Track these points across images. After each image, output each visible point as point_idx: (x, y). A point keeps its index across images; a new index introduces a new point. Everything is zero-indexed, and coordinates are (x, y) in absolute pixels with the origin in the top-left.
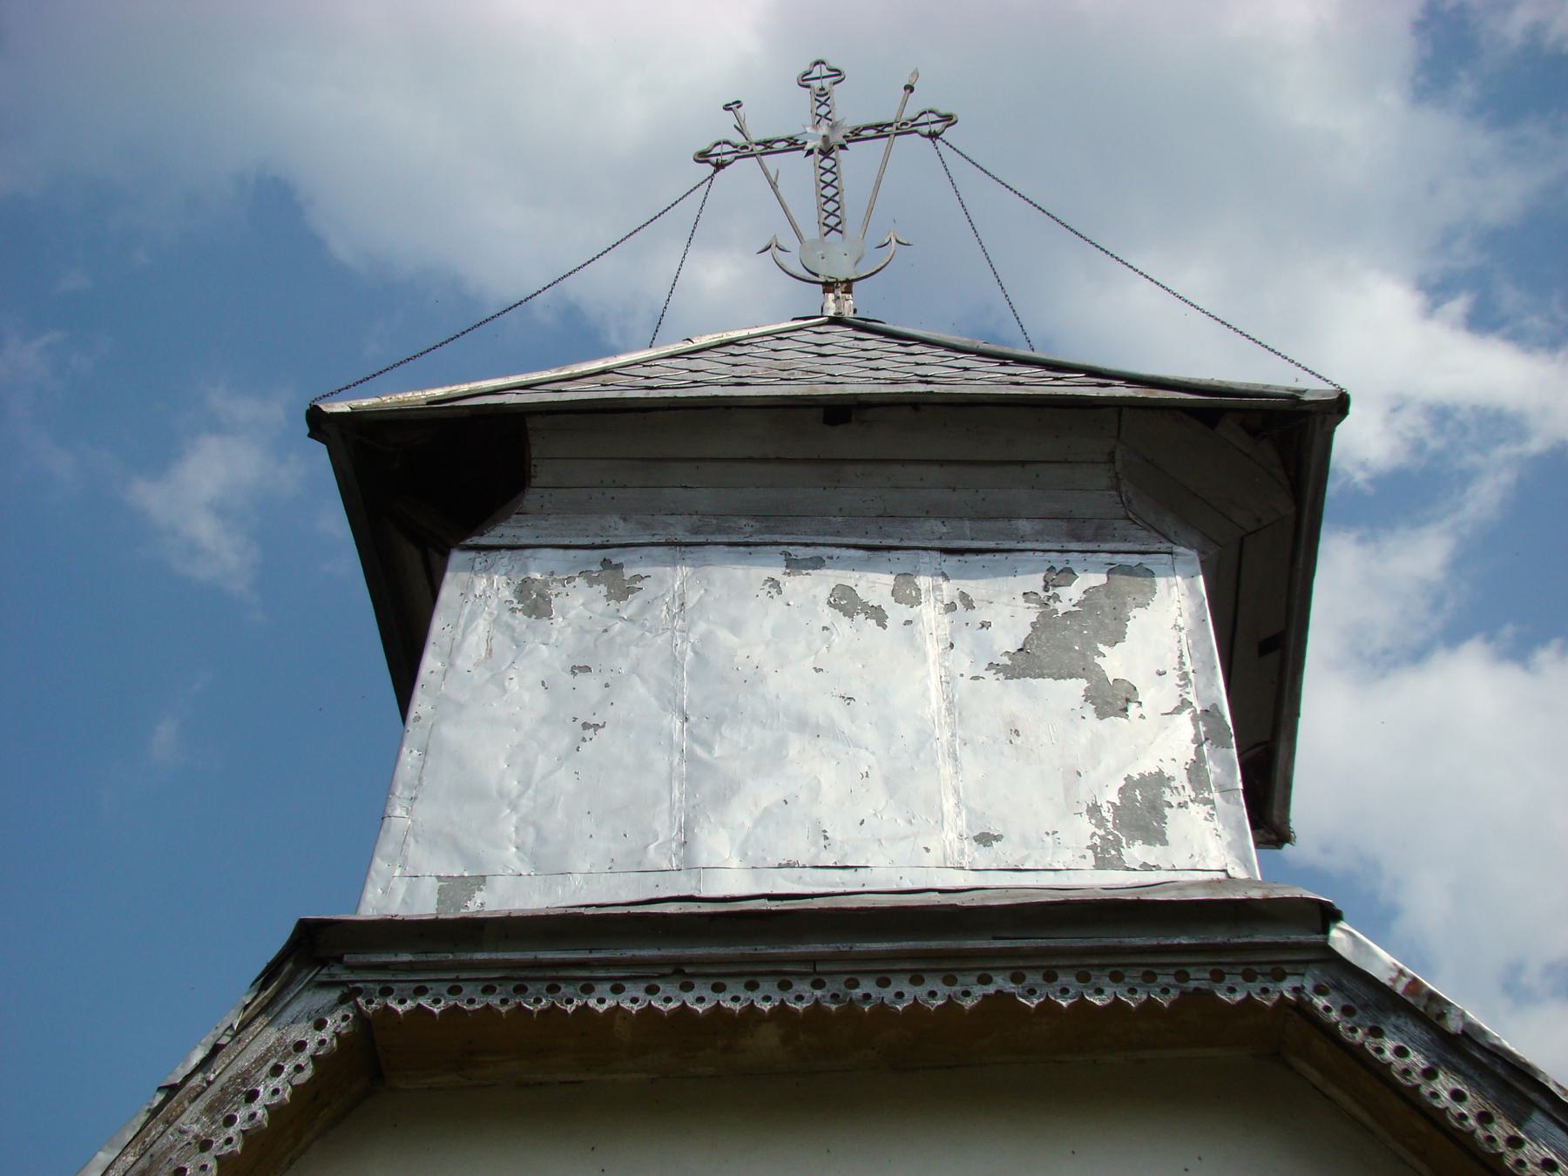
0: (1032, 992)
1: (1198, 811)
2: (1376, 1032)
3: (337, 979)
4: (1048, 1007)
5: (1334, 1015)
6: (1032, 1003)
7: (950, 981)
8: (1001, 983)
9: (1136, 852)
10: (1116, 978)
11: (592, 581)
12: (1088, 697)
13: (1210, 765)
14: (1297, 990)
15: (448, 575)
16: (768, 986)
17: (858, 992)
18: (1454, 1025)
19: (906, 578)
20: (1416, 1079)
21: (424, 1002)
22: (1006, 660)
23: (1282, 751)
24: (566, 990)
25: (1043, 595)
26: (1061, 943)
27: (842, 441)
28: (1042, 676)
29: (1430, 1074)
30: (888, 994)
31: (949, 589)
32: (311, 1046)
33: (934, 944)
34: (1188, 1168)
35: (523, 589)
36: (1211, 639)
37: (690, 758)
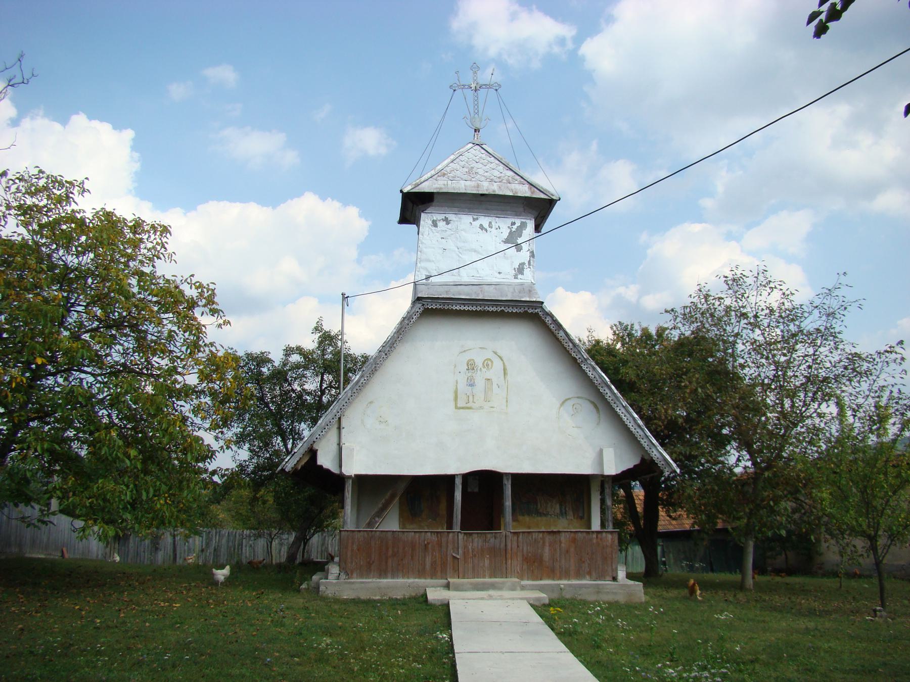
3: (614, 406)
4: (508, 312)
8: (503, 308)
9: (520, 276)
27: (483, 198)
30: (489, 309)
34: (478, 126)
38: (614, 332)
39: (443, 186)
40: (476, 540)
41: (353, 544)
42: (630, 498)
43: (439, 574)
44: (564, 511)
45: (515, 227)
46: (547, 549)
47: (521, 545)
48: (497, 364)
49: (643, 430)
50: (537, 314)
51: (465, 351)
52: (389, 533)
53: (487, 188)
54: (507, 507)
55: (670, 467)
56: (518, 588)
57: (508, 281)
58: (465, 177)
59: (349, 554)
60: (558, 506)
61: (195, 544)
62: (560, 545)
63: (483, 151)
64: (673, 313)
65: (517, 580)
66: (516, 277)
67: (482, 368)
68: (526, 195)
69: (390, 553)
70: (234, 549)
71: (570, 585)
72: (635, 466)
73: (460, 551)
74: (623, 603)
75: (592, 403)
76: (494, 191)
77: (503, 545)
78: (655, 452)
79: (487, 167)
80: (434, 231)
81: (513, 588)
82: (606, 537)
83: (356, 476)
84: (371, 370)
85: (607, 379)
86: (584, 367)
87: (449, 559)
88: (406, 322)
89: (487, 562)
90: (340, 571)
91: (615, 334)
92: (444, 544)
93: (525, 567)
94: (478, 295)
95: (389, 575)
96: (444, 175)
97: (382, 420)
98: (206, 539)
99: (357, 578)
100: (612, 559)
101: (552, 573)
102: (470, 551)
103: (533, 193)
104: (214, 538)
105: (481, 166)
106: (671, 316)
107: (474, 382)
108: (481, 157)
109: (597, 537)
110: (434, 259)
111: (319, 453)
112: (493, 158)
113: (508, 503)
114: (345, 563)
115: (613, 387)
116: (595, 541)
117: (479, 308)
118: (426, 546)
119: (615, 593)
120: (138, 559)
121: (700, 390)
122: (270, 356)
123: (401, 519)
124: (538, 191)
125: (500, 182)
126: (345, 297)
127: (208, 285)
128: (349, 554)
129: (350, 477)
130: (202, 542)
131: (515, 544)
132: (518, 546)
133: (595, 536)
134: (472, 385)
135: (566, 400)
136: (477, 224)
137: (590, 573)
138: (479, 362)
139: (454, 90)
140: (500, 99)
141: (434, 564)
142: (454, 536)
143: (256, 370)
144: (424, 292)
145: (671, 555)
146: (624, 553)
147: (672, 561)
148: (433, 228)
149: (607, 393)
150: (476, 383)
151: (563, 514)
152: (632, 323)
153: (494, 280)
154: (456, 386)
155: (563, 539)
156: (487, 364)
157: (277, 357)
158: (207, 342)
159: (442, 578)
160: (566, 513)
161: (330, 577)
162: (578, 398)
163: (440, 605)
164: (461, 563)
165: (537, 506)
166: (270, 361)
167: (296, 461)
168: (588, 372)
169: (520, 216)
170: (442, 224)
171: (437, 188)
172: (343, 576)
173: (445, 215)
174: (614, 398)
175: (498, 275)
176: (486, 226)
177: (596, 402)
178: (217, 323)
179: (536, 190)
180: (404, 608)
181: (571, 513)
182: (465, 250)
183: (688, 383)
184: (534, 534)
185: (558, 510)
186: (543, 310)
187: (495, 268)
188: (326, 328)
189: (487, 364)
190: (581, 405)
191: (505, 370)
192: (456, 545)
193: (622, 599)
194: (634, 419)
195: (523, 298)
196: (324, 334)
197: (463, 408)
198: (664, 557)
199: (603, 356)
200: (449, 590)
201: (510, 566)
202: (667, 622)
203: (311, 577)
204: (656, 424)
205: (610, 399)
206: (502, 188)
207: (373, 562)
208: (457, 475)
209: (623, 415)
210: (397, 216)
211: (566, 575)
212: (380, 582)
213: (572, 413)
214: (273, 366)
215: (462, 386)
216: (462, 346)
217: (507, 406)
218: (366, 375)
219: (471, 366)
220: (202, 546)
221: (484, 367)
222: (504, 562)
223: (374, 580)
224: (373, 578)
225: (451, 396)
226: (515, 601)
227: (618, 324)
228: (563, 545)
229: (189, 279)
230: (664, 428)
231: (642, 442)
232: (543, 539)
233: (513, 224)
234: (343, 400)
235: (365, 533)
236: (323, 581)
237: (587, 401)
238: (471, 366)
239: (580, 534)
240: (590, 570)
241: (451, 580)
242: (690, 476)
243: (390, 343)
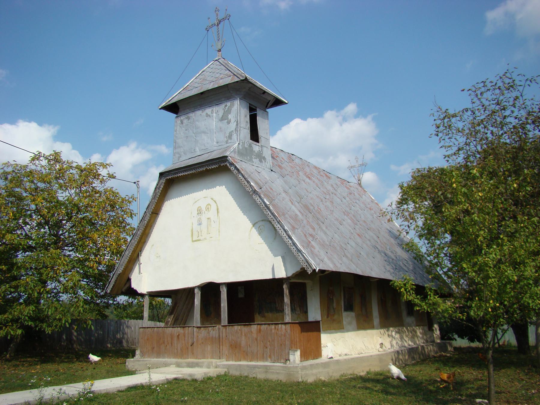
9: (229, 141)
27: (203, 96)
48: (214, 207)
77: (217, 335)
118: (178, 336)
119: (278, 373)
131: (224, 335)
135: (257, 223)
136: (204, 114)
140: (232, 27)
148: (181, 125)
156: (208, 208)
162: (262, 221)
165: (276, 304)
170: (185, 121)
176: (209, 113)
181: (298, 309)
189: (208, 208)
191: (218, 209)
197: (196, 241)
221: (206, 210)
233: (226, 106)
238: (200, 212)
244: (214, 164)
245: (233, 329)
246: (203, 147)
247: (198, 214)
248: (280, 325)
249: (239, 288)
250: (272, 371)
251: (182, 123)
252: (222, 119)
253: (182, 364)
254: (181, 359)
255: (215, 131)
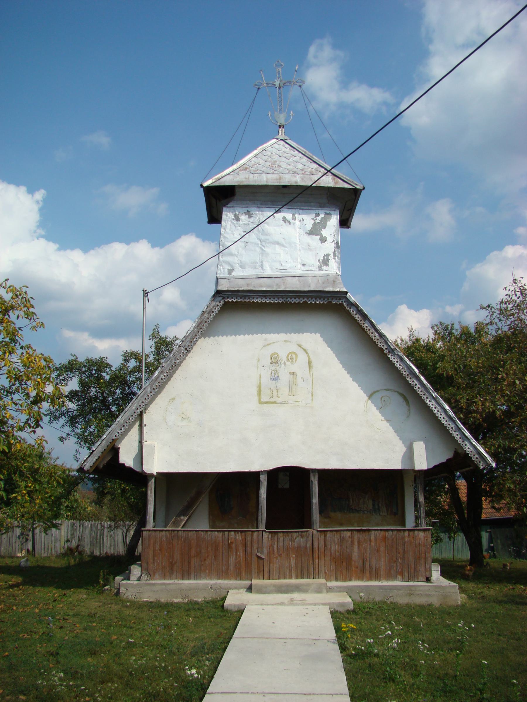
0: (309, 301)
1: (334, 260)
2: (350, 308)
3: (424, 397)
5: (346, 306)
6: (309, 302)
7: (299, 299)
9: (324, 268)
10: (320, 299)
11: (246, 214)
12: (320, 239)
13: (336, 252)
14: (342, 302)
15: (223, 213)
16: (276, 299)
17: (288, 300)
18: (359, 309)
19: (294, 215)
20: (354, 315)
21: (233, 300)
22: (308, 232)
23: (350, 219)
24: (251, 298)
25: (314, 218)
26: (313, 295)
27: (285, 190)
28: (313, 235)
29: (356, 314)
30: (291, 300)
31: (301, 217)
32: (219, 305)
33: (298, 295)
35: (235, 215)
36: (324, 528)
37: (262, 250)
38: (436, 331)
39: (244, 180)
40: (282, 538)
41: (155, 543)
42: (454, 490)
43: (244, 575)
44: (377, 507)
45: (319, 218)
46: (356, 548)
47: (328, 543)
48: (302, 358)
49: (455, 422)
50: (341, 305)
51: (268, 345)
52: (192, 532)
53: (288, 180)
54: (314, 504)
55: (486, 461)
56: (325, 590)
57: (312, 272)
58: (268, 170)
59: (151, 553)
60: (371, 502)
61: (61, 535)
62: (370, 544)
63: (287, 146)
64: (489, 309)
65: (323, 581)
66: (320, 268)
67: (287, 363)
68: (329, 185)
69: (193, 552)
70: (97, 539)
71: (380, 587)
72: (448, 460)
73: (265, 551)
74: (437, 606)
75: (401, 395)
76: (296, 182)
77: (309, 544)
78: (468, 445)
79: (291, 160)
80: (237, 225)
81: (319, 591)
82: (419, 535)
83: (158, 473)
84: (170, 365)
85: (416, 370)
86: (391, 358)
87: (254, 559)
88: (206, 315)
89: (293, 562)
90: (141, 571)
91: (436, 333)
92: (248, 544)
93: (333, 567)
94: (280, 287)
95: (193, 576)
96: (246, 169)
97: (184, 417)
98: (71, 531)
99: (159, 579)
100: (425, 558)
101: (362, 574)
102: (276, 550)
103: (336, 183)
104: (78, 529)
105: (284, 159)
106: (488, 311)
107: (278, 376)
108: (284, 152)
109: (409, 535)
110: (236, 253)
111: (121, 451)
112: (296, 152)
113: (315, 500)
114: (148, 563)
115: (422, 378)
116: (406, 539)
117: (281, 301)
118: (230, 546)
119: (428, 596)
120: (11, 548)
121: (517, 382)
122: (108, 361)
123: (211, 517)
124: (342, 182)
125: (303, 174)
126: (146, 293)
127: (21, 288)
128: (151, 553)
129: (152, 475)
130: (68, 533)
131: (322, 544)
132: (325, 545)
133: (406, 534)
134: (276, 379)
135: (374, 392)
137: (401, 573)
138: (283, 355)
139: (258, 89)
141: (237, 564)
142: (259, 535)
143: (96, 375)
144: (224, 285)
145: (499, 541)
146: (452, 540)
147: (500, 547)
148: (235, 222)
149: (416, 385)
150: (280, 377)
151: (376, 510)
152: (453, 322)
153: (299, 272)
154: (260, 381)
155: (372, 537)
156: (292, 357)
157: (116, 362)
158: (23, 344)
159: (246, 579)
160: (379, 509)
161: (132, 578)
163: (236, 611)
164: (266, 563)
166: (108, 366)
167: (95, 460)
168: (395, 362)
169: (324, 207)
171: (238, 182)
172: (144, 577)
173: (247, 209)
174: (423, 389)
175: (303, 268)
177: (406, 395)
178: (31, 326)
179: (339, 180)
180: (199, 614)
182: (268, 243)
183: (505, 375)
184: (342, 532)
185: (371, 507)
186: (347, 300)
187: (299, 260)
188: (162, 334)
189: (292, 357)
190: (390, 398)
191: (310, 363)
192: (261, 545)
193: (435, 601)
194: (445, 411)
195: (326, 288)
196: (160, 339)
197: (266, 403)
198: (492, 543)
199: (422, 352)
200: (251, 592)
201: (317, 566)
202: (483, 634)
203: (114, 578)
204: (474, 418)
205: (420, 390)
206: (305, 179)
207: (176, 563)
208: (262, 471)
209: (433, 407)
210: (206, 219)
211: (376, 575)
212: (181, 584)
213: (380, 405)
214: (112, 370)
215: (266, 380)
216: (266, 340)
217: (312, 400)
218: (165, 371)
219: (275, 360)
220: (68, 536)
221: (288, 360)
222: (311, 562)
223: (176, 581)
224: (176, 579)
225: (255, 391)
226: (317, 607)
227: (439, 324)
228: (373, 544)
229: (4, 284)
230: (483, 421)
231: (455, 434)
232: (352, 537)
234: (143, 396)
235: (167, 533)
236: (124, 582)
237: (396, 394)
238: (275, 360)
239: (390, 532)
240: (402, 570)
241: (255, 582)
242: (512, 468)
243: (189, 337)
244: (320, 298)
245: (338, 535)
246: (277, 266)
247: (271, 363)
248: (416, 532)
249: (311, 475)
250: (420, 592)
251: (237, 219)
252: (311, 233)
253: (266, 587)
254: (206, 579)
255: (298, 246)
